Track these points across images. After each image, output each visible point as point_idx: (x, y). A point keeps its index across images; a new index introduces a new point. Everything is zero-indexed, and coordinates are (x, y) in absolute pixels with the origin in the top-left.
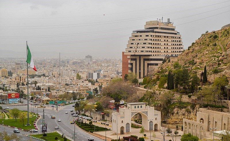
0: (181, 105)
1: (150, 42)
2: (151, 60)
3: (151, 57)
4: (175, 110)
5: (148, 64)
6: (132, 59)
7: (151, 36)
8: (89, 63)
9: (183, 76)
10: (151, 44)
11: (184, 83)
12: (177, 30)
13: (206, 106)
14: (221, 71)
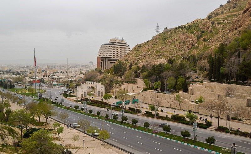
0: (117, 82)
1: (111, 50)
2: (112, 60)
3: (112, 59)
4: (114, 85)
5: (110, 63)
6: (101, 60)
7: (112, 47)
8: (91, 66)
9: (119, 67)
10: (112, 51)
11: (119, 70)
12: (128, 44)
13: (127, 82)
14: (139, 63)
